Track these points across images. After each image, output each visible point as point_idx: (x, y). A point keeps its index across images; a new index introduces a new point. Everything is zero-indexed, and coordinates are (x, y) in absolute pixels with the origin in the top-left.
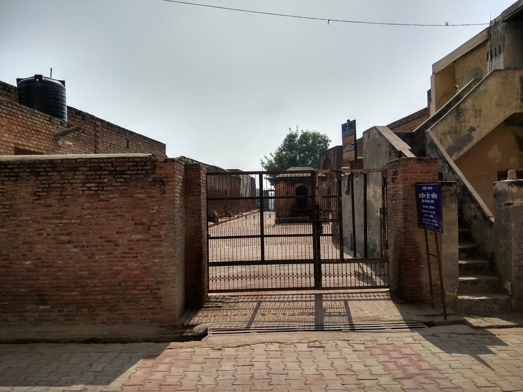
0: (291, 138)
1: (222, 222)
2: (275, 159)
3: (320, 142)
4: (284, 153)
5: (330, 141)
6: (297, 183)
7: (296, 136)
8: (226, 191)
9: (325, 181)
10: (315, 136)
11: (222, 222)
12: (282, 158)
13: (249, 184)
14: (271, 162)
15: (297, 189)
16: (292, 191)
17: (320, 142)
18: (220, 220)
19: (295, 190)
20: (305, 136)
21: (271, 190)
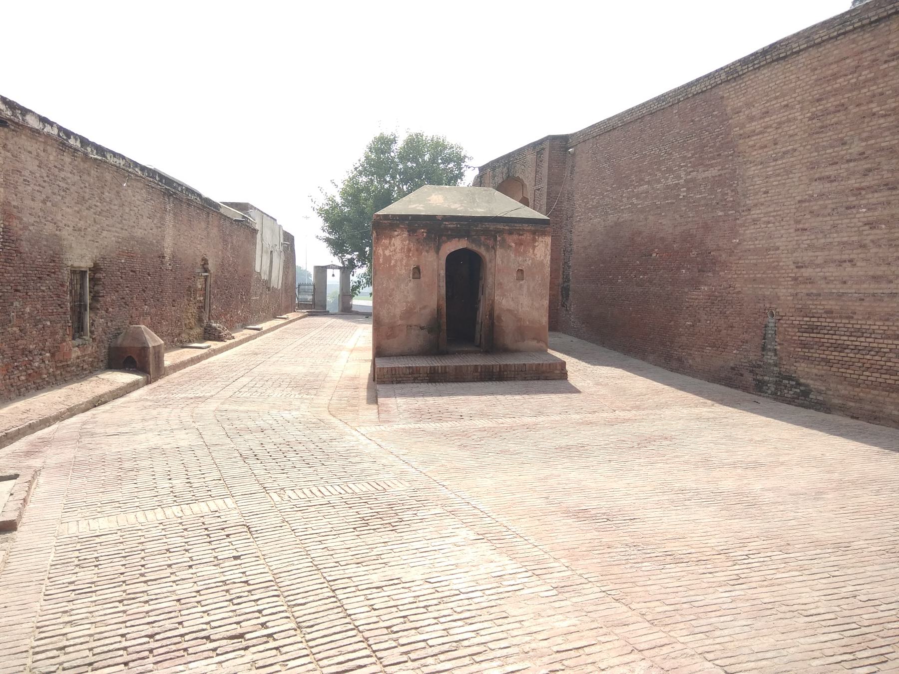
0: (383, 144)
1: (176, 367)
2: (344, 193)
3: (447, 161)
4: (364, 179)
5: (471, 159)
6: (450, 238)
7: (394, 141)
8: (205, 261)
9: (543, 234)
10: (438, 147)
11: (176, 367)
12: (360, 191)
13: (279, 248)
14: (334, 201)
15: (452, 258)
16: (434, 264)
17: (447, 161)
18: (169, 359)
19: (443, 262)
20: (414, 146)
21: (333, 267)
